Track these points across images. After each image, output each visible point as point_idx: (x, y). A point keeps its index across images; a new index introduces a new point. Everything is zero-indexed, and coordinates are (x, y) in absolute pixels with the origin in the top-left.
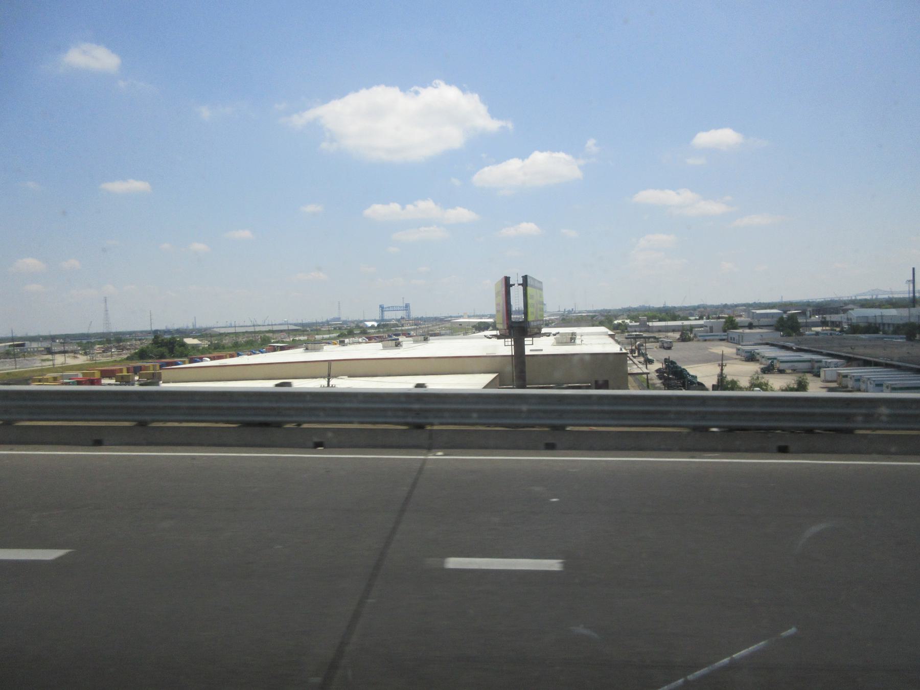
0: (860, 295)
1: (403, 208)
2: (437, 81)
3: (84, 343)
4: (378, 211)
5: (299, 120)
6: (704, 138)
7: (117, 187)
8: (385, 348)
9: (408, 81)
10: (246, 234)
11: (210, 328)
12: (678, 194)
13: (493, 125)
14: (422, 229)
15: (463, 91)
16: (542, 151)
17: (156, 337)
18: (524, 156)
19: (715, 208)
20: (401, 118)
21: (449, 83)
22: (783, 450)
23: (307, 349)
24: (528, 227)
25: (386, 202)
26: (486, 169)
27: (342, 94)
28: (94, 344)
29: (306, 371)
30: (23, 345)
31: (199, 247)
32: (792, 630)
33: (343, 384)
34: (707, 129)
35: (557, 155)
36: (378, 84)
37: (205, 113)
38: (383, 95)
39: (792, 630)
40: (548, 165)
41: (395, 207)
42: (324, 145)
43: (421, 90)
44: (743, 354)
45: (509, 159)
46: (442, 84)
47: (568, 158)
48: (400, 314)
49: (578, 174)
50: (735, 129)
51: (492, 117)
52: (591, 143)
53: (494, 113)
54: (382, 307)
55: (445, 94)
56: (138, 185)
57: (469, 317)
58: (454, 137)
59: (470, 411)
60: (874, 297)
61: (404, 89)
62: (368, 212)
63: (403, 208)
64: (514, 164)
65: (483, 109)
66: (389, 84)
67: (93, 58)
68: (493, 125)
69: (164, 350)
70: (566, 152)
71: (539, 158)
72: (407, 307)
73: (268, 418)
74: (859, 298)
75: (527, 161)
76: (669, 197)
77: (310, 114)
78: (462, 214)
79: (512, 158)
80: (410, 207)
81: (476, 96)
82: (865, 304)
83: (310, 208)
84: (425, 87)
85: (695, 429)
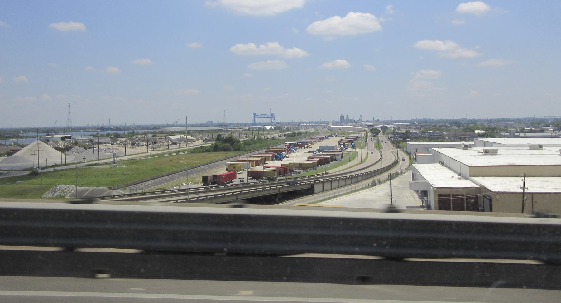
1: (258, 47)
4: (240, 48)
6: (464, 7)
7: (62, 26)
14: (269, 62)
16: (354, 11)
18: (343, 15)
19: (470, 54)
24: (341, 62)
35: (364, 14)
41: (252, 46)
47: (373, 17)
49: (379, 27)
52: (389, 7)
54: (255, 115)
56: (78, 26)
59: (528, 132)
62: (233, 49)
64: (336, 20)
71: (353, 16)
72: (272, 115)
75: (344, 19)
76: (439, 45)
78: (297, 52)
79: (334, 16)
80: (262, 46)
85: (389, 258)
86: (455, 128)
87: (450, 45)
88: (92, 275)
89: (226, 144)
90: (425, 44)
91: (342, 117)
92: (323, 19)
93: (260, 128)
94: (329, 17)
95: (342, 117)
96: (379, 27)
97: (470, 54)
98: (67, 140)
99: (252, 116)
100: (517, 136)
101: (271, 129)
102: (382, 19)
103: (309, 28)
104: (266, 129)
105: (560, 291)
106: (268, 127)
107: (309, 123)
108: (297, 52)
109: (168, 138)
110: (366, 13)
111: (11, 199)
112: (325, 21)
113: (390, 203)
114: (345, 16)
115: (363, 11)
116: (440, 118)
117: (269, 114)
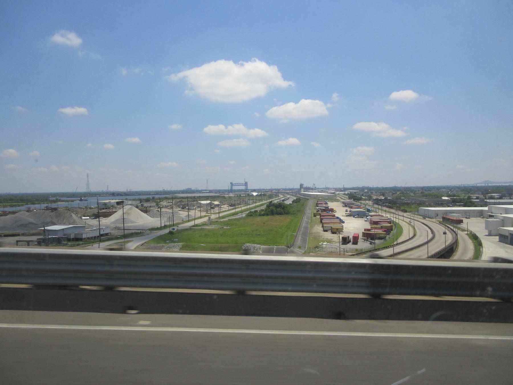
0: (478, 183)
1: (226, 128)
3: (220, 196)
4: (212, 129)
5: (175, 78)
6: (396, 95)
7: (69, 111)
9: (239, 57)
10: (136, 140)
12: (378, 125)
14: (235, 140)
15: (269, 64)
16: (306, 99)
18: (297, 102)
19: (399, 133)
20: (229, 79)
21: (261, 59)
24: (293, 141)
25: (216, 124)
26: (274, 108)
31: (110, 146)
32: (423, 370)
35: (313, 101)
36: (212, 61)
37: (124, 72)
38: (230, 64)
39: (423, 370)
40: (310, 107)
41: (222, 127)
42: (186, 92)
43: (245, 63)
46: (257, 60)
48: (243, 188)
49: (326, 112)
51: (284, 80)
52: (335, 95)
53: (285, 77)
54: (231, 183)
55: (259, 66)
56: (82, 110)
58: (261, 90)
60: (486, 185)
61: (236, 62)
62: (206, 129)
64: (291, 106)
65: (279, 75)
66: (227, 59)
70: (320, 100)
71: (305, 103)
72: (246, 184)
74: (478, 185)
75: (298, 105)
77: (181, 75)
78: (258, 132)
79: (289, 102)
80: (230, 127)
81: (276, 67)
82: (183, 192)
83: (175, 127)
84: (247, 62)
86: (412, 194)
87: (383, 126)
88: (124, 310)
92: (282, 104)
93: (248, 195)
96: (326, 112)
97: (399, 133)
98: (147, 201)
99: (230, 185)
101: (257, 195)
102: (329, 105)
104: (252, 195)
106: (255, 194)
107: (285, 189)
108: (258, 132)
111: (498, 185)
112: (282, 106)
114: (298, 103)
117: (244, 183)
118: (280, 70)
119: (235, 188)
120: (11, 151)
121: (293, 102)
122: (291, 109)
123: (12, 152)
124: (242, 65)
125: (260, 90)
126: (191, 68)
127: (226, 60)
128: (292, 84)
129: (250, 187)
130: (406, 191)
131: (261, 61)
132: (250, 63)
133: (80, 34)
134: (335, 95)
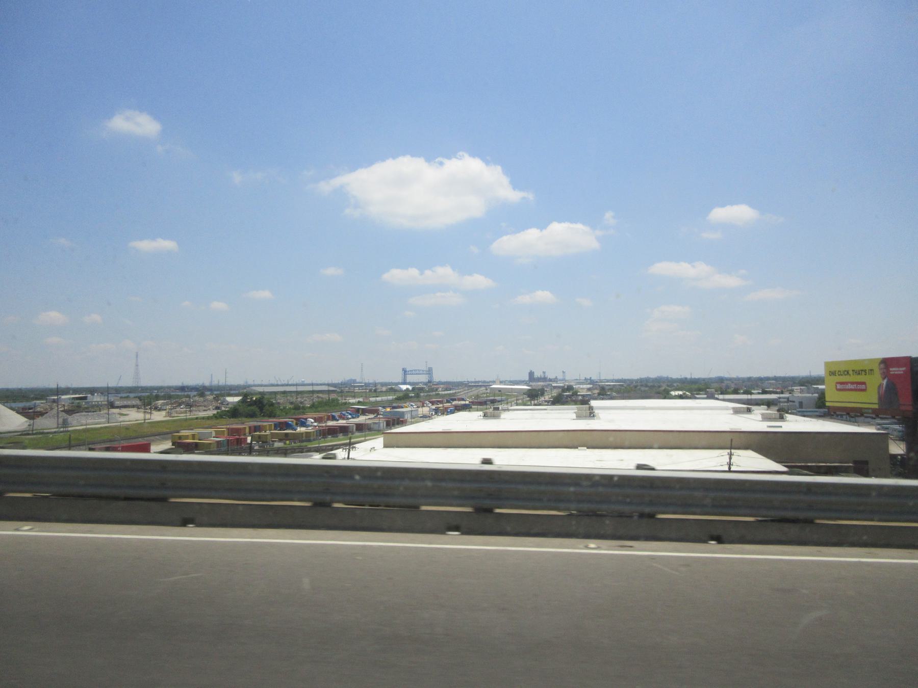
1: (422, 274)
2: (461, 153)
4: (397, 275)
5: (326, 187)
6: (720, 214)
7: (145, 245)
8: (579, 417)
9: (434, 151)
10: (266, 294)
11: (249, 386)
12: (693, 266)
13: (512, 195)
14: (438, 294)
15: (487, 163)
16: (560, 222)
17: (245, 396)
18: (542, 226)
19: (731, 281)
20: (420, 187)
21: (473, 154)
22: (91, 449)
23: (485, 416)
24: (544, 295)
26: (505, 238)
27: (368, 161)
28: (310, 408)
29: (535, 444)
30: (85, 398)
31: (219, 305)
33: (507, 460)
34: (723, 205)
36: (404, 155)
37: (237, 177)
38: (407, 165)
40: (565, 235)
41: (414, 272)
43: (445, 161)
44: (895, 433)
45: (527, 228)
46: (466, 156)
48: (424, 378)
49: (595, 245)
50: (752, 205)
51: (514, 189)
52: (609, 215)
53: (516, 185)
57: (501, 382)
58: (475, 207)
61: (429, 159)
62: (386, 276)
63: (422, 274)
64: (532, 234)
65: (505, 180)
67: (136, 125)
68: (512, 195)
69: (254, 408)
70: (584, 223)
71: (558, 229)
72: (430, 372)
73: (487, 501)
75: (545, 232)
77: (337, 181)
78: (479, 281)
79: (531, 228)
80: (428, 273)
81: (499, 168)
83: (331, 271)
84: (449, 158)
89: (252, 408)
90: (664, 268)
91: (531, 374)
94: (523, 230)
95: (531, 374)
96: (595, 245)
99: (401, 373)
100: (717, 399)
103: (495, 245)
105: (2, 390)
109: (225, 400)
110: (576, 223)
112: (518, 235)
113: (351, 452)
115: (571, 218)
116: (644, 375)
118: (507, 171)
119: (410, 378)
120: (54, 314)
121: (538, 228)
122: (531, 241)
123: (54, 316)
124: (441, 164)
125: (475, 206)
126: (353, 168)
127: (412, 156)
128: (531, 196)
129: (437, 378)
130: (659, 381)
131: (474, 157)
132: (454, 160)
133: (156, 115)
134: (609, 215)
